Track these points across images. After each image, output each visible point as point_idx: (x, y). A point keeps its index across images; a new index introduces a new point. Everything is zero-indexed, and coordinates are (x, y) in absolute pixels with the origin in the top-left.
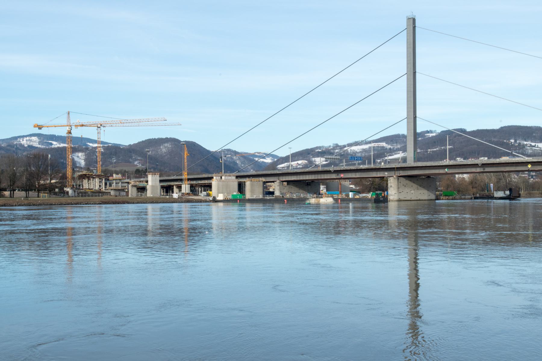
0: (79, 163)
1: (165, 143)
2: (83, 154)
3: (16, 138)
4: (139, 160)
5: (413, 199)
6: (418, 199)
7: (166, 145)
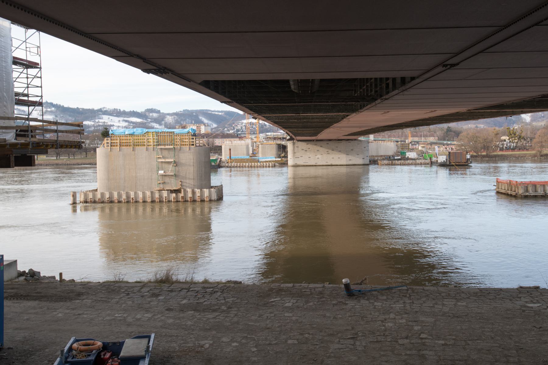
5: (318, 164)
6: (329, 164)
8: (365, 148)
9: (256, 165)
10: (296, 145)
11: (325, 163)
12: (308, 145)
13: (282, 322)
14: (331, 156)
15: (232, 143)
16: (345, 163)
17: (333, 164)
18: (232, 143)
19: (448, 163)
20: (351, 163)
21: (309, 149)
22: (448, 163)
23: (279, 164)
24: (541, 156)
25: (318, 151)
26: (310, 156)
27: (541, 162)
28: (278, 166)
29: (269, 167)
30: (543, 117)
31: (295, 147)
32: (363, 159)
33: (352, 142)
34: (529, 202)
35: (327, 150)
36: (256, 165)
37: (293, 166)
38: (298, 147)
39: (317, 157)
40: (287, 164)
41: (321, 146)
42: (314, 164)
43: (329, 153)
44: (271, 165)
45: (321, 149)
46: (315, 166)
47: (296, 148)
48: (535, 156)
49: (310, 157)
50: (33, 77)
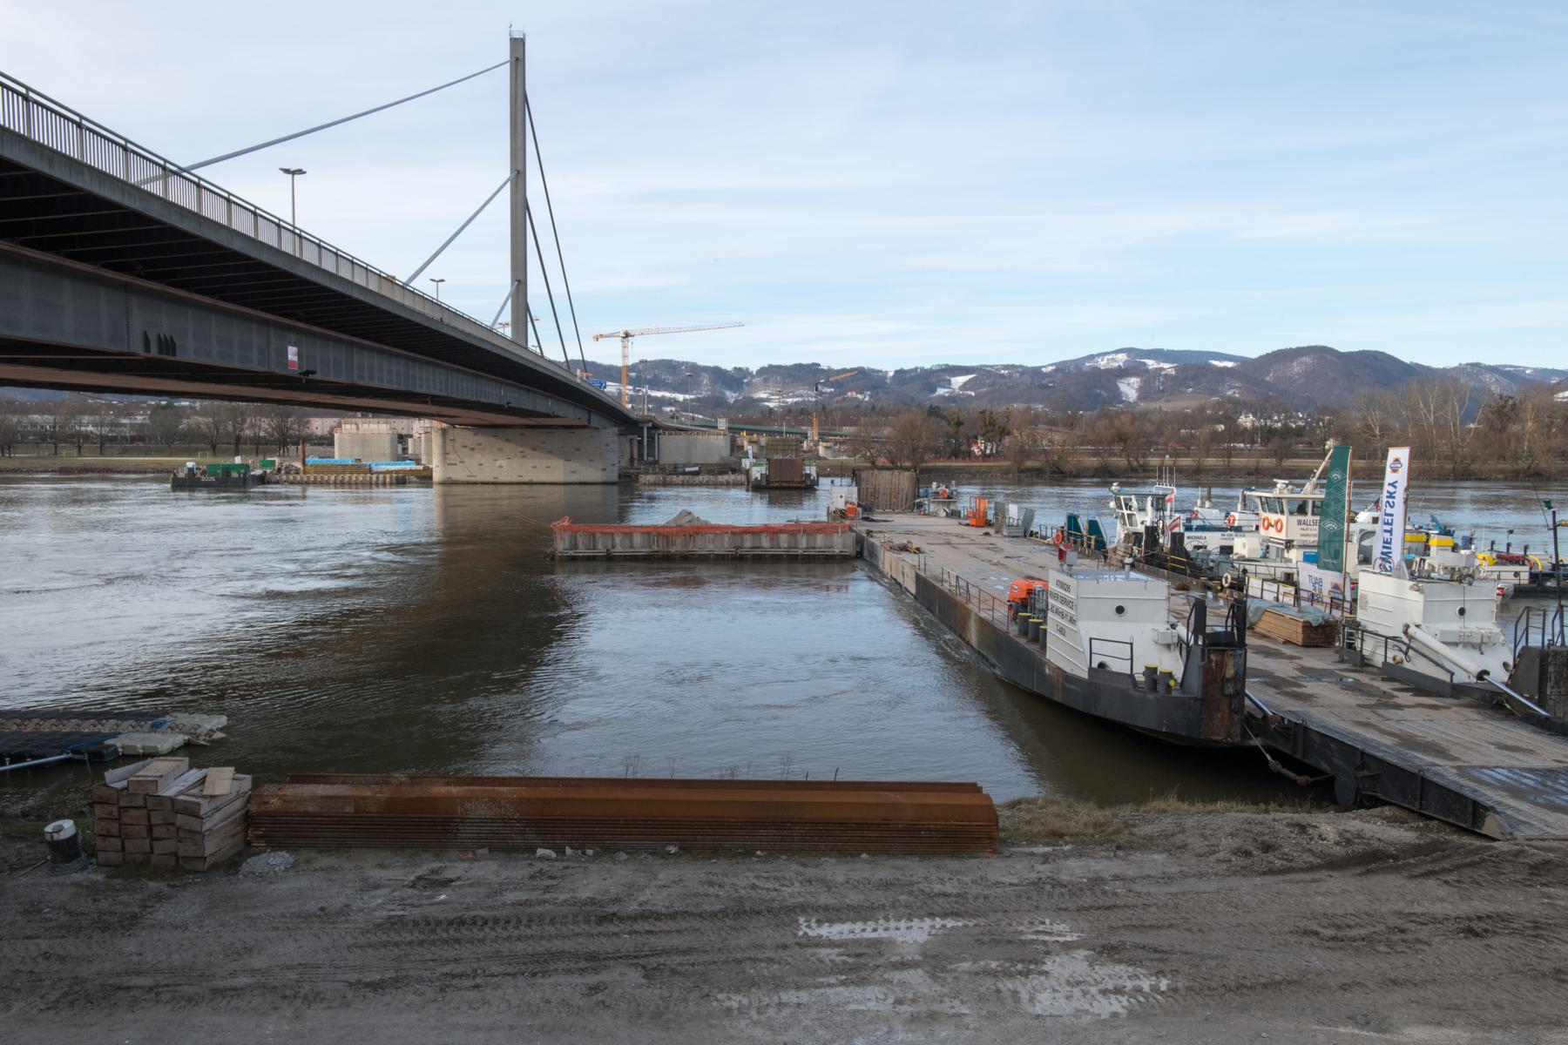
0: (1127, 395)
1: (1302, 356)
2: (1138, 380)
3: (1091, 357)
4: (1235, 387)
5: (502, 479)
7: (1303, 359)
8: (607, 445)
9: (354, 479)
10: (450, 436)
11: (515, 479)
12: (477, 437)
13: (129, 905)
14: (529, 463)
15: (358, 429)
16: (561, 479)
17: (535, 480)
18: (358, 429)
19: (764, 483)
20: (574, 478)
21: (480, 444)
22: (764, 483)
23: (418, 477)
24: (1022, 471)
25: (500, 449)
26: (483, 461)
27: (1019, 484)
28: (415, 482)
29: (384, 484)
30: (1163, 392)
31: (448, 442)
32: (604, 470)
33: (578, 432)
34: (802, 568)
35: (522, 449)
36: (354, 479)
37: (442, 483)
38: (454, 440)
39: (498, 463)
40: (431, 478)
41: (508, 440)
42: (492, 480)
43: (524, 457)
44: (388, 480)
45: (507, 446)
46: (494, 483)
47: (449, 444)
48: (1007, 471)
49: (481, 465)
50: (297, 239)
